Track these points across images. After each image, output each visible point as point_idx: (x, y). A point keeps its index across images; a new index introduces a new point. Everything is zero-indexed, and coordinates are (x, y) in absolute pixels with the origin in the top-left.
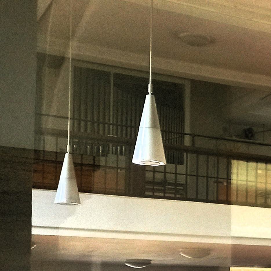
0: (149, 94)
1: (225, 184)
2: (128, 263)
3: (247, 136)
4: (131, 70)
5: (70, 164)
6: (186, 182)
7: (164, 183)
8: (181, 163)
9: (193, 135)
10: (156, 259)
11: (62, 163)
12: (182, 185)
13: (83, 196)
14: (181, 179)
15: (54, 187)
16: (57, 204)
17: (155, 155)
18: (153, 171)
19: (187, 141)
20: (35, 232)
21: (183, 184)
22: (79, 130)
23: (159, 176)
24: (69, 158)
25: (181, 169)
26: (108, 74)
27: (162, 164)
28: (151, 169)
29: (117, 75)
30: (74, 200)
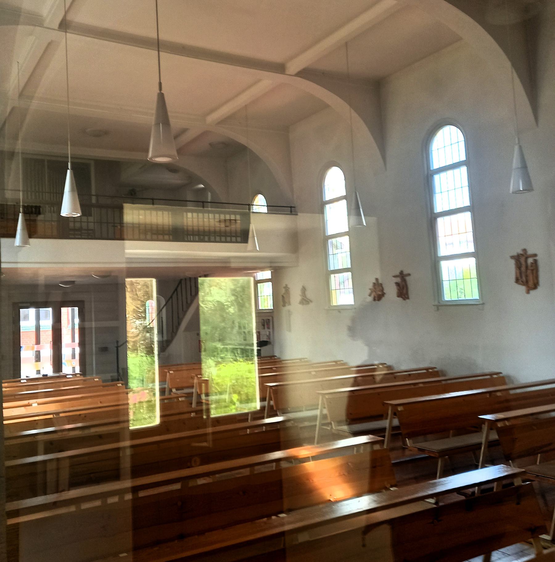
0: (69, 169)
1: (119, 227)
2: (60, 284)
3: (132, 195)
4: (57, 156)
5: (22, 218)
6: (94, 227)
7: (80, 229)
8: (91, 215)
9: (97, 196)
10: (78, 280)
11: (18, 219)
12: (92, 230)
13: (32, 241)
14: (91, 226)
15: (14, 236)
16: (18, 248)
17: (74, 210)
18: (74, 222)
19: (94, 200)
20: (3, 266)
21: (92, 229)
22: (28, 198)
23: (78, 225)
24: (22, 216)
25: (91, 219)
26: (43, 161)
27: (79, 215)
28: (72, 220)
29: (49, 161)
30: (25, 242)
